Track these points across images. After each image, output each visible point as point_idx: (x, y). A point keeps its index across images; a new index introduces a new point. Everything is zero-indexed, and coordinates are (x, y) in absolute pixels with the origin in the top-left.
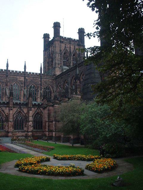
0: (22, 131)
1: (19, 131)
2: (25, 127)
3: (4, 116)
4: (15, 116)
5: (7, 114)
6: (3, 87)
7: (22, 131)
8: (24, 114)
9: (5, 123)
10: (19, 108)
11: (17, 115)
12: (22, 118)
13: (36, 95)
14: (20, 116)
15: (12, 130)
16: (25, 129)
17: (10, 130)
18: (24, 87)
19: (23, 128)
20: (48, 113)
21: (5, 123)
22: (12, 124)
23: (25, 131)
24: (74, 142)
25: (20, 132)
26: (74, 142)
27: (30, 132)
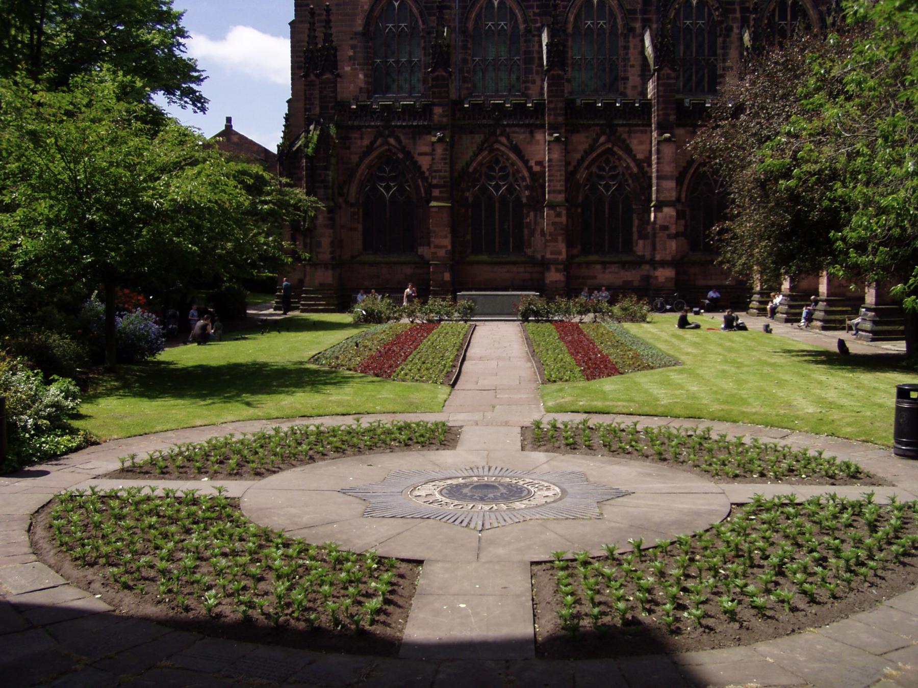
0: (626, 258)
1: (607, 259)
2: (640, 238)
3: (524, 179)
4: (582, 175)
5: (537, 169)
6: (525, 21)
7: (626, 258)
8: (632, 165)
9: (532, 214)
10: (603, 133)
11: (594, 169)
12: (620, 187)
13: (715, 54)
14: (613, 178)
15: (564, 251)
16: (641, 248)
17: (552, 253)
18: (644, 11)
19: (628, 245)
20: (331, 28)
21: (532, 214)
22: (563, 219)
23: (639, 262)
24: (880, 328)
25: (614, 268)
26: (880, 328)
27: (663, 264)
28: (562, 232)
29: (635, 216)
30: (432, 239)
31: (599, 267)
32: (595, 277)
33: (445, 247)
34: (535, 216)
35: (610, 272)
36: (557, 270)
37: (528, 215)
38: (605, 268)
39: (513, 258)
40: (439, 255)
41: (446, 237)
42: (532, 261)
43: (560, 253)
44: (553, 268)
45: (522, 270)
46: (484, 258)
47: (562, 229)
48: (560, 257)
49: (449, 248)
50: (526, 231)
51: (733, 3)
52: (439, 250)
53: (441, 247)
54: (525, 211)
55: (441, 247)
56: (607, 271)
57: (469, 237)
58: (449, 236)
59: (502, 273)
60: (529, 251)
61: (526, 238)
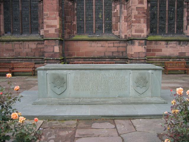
9: (118, 7)
21: (118, 7)
25: (173, 44)
28: (144, 15)
29: (185, 10)
30: (44, 21)
31: (163, 43)
32: (161, 50)
33: (55, 26)
34: (121, 8)
35: (171, 47)
36: (140, 44)
37: (115, 8)
38: (167, 44)
39: (105, 37)
40: (50, 32)
41: (56, 19)
42: (119, 40)
43: (142, 31)
44: (137, 42)
45: (112, 45)
46: (85, 37)
47: (144, 13)
48: (142, 34)
49: (58, 27)
50: (114, 19)
51: (26, 141)
52: (50, 29)
53: (52, 26)
54: (113, 5)
55: (52, 26)
56: (169, 46)
57: (75, 23)
58: (58, 18)
59: (97, 48)
60: (116, 33)
61: (113, 23)
